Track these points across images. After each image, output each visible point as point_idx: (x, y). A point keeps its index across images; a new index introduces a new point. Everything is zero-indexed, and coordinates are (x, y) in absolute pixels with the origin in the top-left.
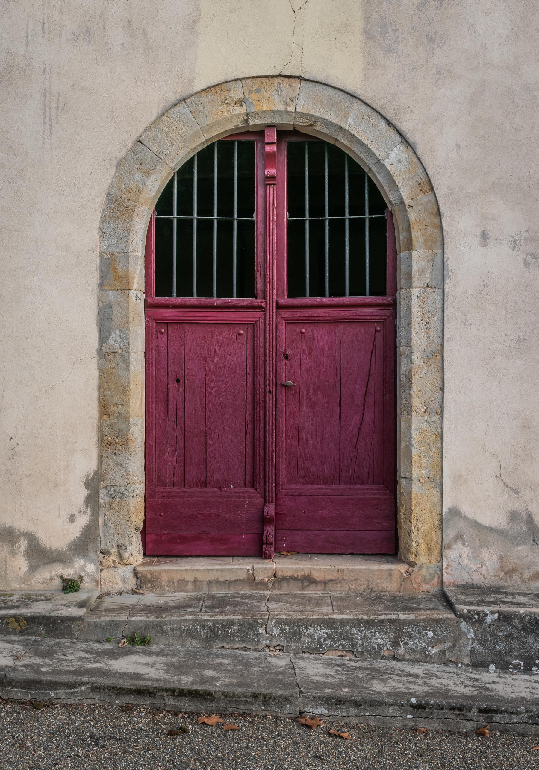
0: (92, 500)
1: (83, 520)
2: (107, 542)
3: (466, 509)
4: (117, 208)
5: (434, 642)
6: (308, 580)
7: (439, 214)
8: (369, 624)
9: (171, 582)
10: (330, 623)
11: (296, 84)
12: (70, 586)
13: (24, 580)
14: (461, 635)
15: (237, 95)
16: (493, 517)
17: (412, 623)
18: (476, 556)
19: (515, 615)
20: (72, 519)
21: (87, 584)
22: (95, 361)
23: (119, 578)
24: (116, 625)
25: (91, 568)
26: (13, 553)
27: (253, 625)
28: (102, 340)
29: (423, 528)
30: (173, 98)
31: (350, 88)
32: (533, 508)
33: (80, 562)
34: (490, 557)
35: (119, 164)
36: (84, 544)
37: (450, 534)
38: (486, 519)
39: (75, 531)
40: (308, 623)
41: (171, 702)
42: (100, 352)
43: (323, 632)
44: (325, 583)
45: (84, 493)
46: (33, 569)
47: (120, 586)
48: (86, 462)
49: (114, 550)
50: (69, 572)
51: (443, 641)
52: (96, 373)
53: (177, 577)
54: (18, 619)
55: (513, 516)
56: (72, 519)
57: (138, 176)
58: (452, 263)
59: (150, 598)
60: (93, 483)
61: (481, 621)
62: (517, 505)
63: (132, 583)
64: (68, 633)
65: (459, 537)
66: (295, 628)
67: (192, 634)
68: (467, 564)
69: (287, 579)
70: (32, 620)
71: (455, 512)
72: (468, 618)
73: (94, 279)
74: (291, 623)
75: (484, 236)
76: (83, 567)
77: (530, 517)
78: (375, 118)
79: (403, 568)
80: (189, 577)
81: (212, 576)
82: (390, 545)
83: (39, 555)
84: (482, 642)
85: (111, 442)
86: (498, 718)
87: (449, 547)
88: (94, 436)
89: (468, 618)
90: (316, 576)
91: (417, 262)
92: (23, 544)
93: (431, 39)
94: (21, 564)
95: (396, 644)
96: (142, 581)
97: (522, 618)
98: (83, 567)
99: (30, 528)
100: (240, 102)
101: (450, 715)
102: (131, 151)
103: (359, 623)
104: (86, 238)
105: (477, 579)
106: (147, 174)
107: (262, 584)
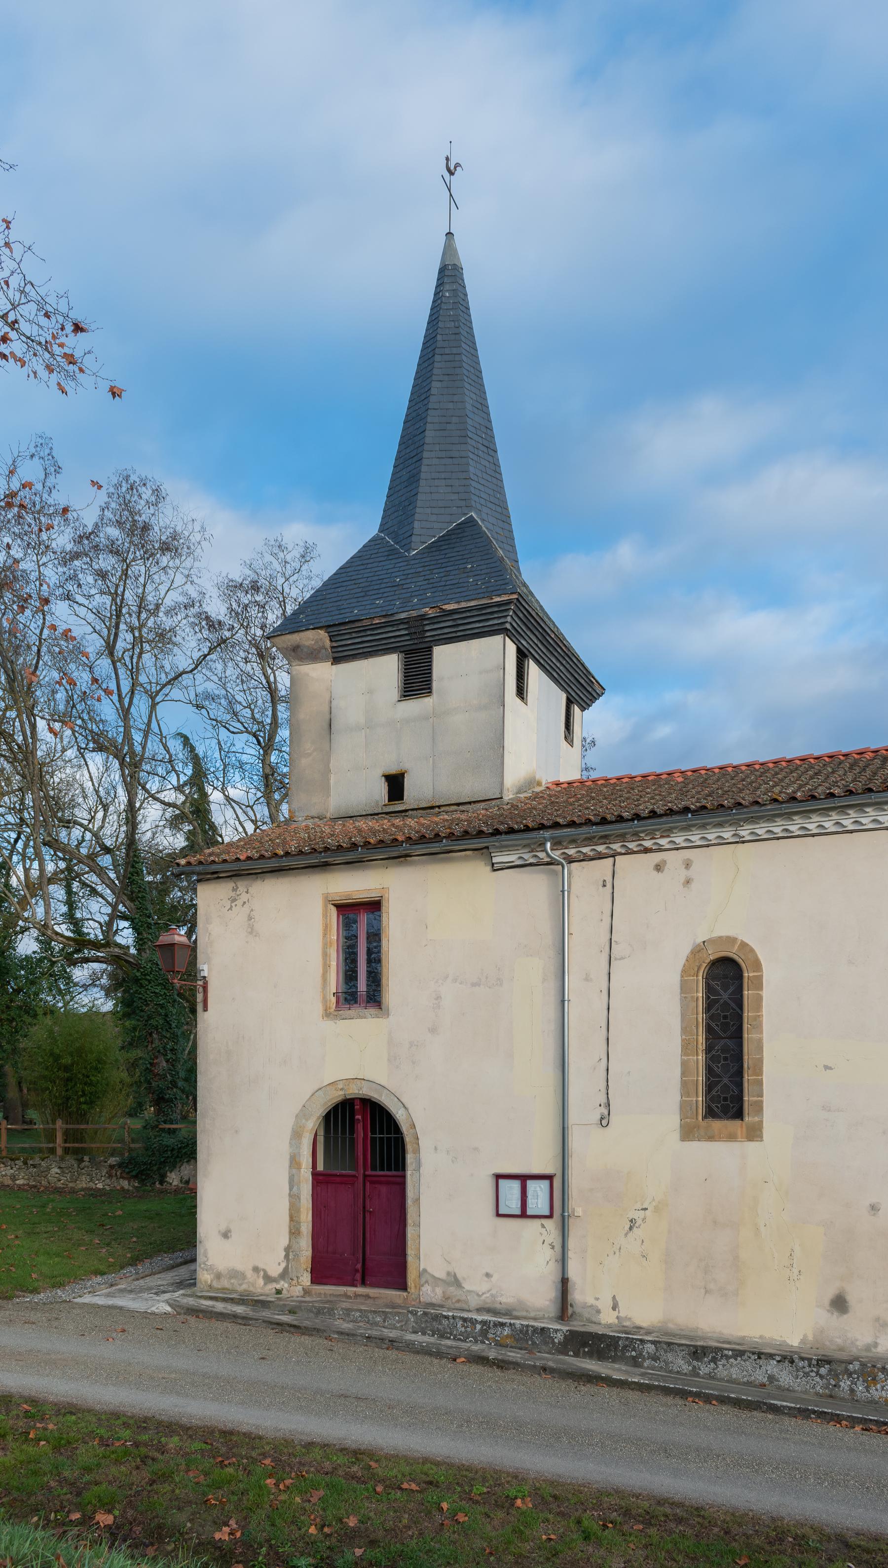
0: (287, 1257)
1: (283, 1265)
2: (293, 1274)
3: (429, 1270)
4: (297, 1135)
5: (399, 1322)
6: (367, 1297)
7: (418, 1138)
8: (375, 1312)
9: (316, 1294)
10: (360, 1311)
11: (363, 1082)
12: (279, 1292)
13: (262, 1288)
14: (408, 1320)
15: (340, 1086)
16: (441, 1274)
17: (390, 1313)
18: (433, 1291)
19: (429, 1313)
20: (279, 1264)
21: (284, 1292)
22: (287, 1198)
23: (297, 1291)
24: (285, 1305)
25: (286, 1285)
26: (258, 1277)
27: (333, 1309)
28: (291, 1190)
29: (413, 1277)
30: (316, 1088)
31: (382, 1084)
32: (456, 1271)
33: (282, 1282)
34: (439, 1291)
35: (297, 1116)
36: (284, 1275)
37: (423, 1280)
38: (437, 1275)
39: (280, 1269)
40: (352, 1310)
41: (288, 1328)
42: (290, 1195)
43: (358, 1314)
44: (374, 1298)
45: (284, 1253)
46: (265, 1284)
47: (298, 1294)
48: (285, 1241)
49: (295, 1279)
50: (278, 1287)
51: (402, 1321)
52: (288, 1204)
53: (318, 1292)
54: (252, 1300)
55: (448, 1274)
56: (279, 1264)
57: (304, 1121)
58: (423, 1161)
59: (307, 1299)
60: (287, 1250)
61: (416, 1314)
62: (450, 1269)
63: (302, 1293)
64: (269, 1308)
65: (427, 1282)
66: (348, 1311)
67: (312, 1312)
68: (430, 1293)
69: (360, 1295)
70: (256, 1301)
71: (425, 1270)
72: (411, 1312)
73: (287, 1164)
74: (347, 1310)
75: (436, 1149)
76: (283, 1285)
77: (455, 1274)
78: (393, 1097)
79: (405, 1294)
80: (322, 1292)
81: (331, 1292)
82: (403, 1286)
83: (268, 1279)
84: (416, 1323)
85: (294, 1232)
86: (395, 1344)
87: (423, 1286)
88: (287, 1230)
89: (411, 1312)
90: (371, 1295)
91: (410, 1158)
92: (262, 1273)
93: (414, 1063)
94: (261, 1282)
95: (384, 1321)
96: (306, 1292)
97: (432, 1314)
98: (283, 1285)
99: (264, 1267)
100: (342, 1089)
101: (379, 1341)
102: (301, 1110)
103: (371, 1311)
104: (282, 1146)
105: (434, 1301)
106: (307, 1120)
107: (350, 1297)
